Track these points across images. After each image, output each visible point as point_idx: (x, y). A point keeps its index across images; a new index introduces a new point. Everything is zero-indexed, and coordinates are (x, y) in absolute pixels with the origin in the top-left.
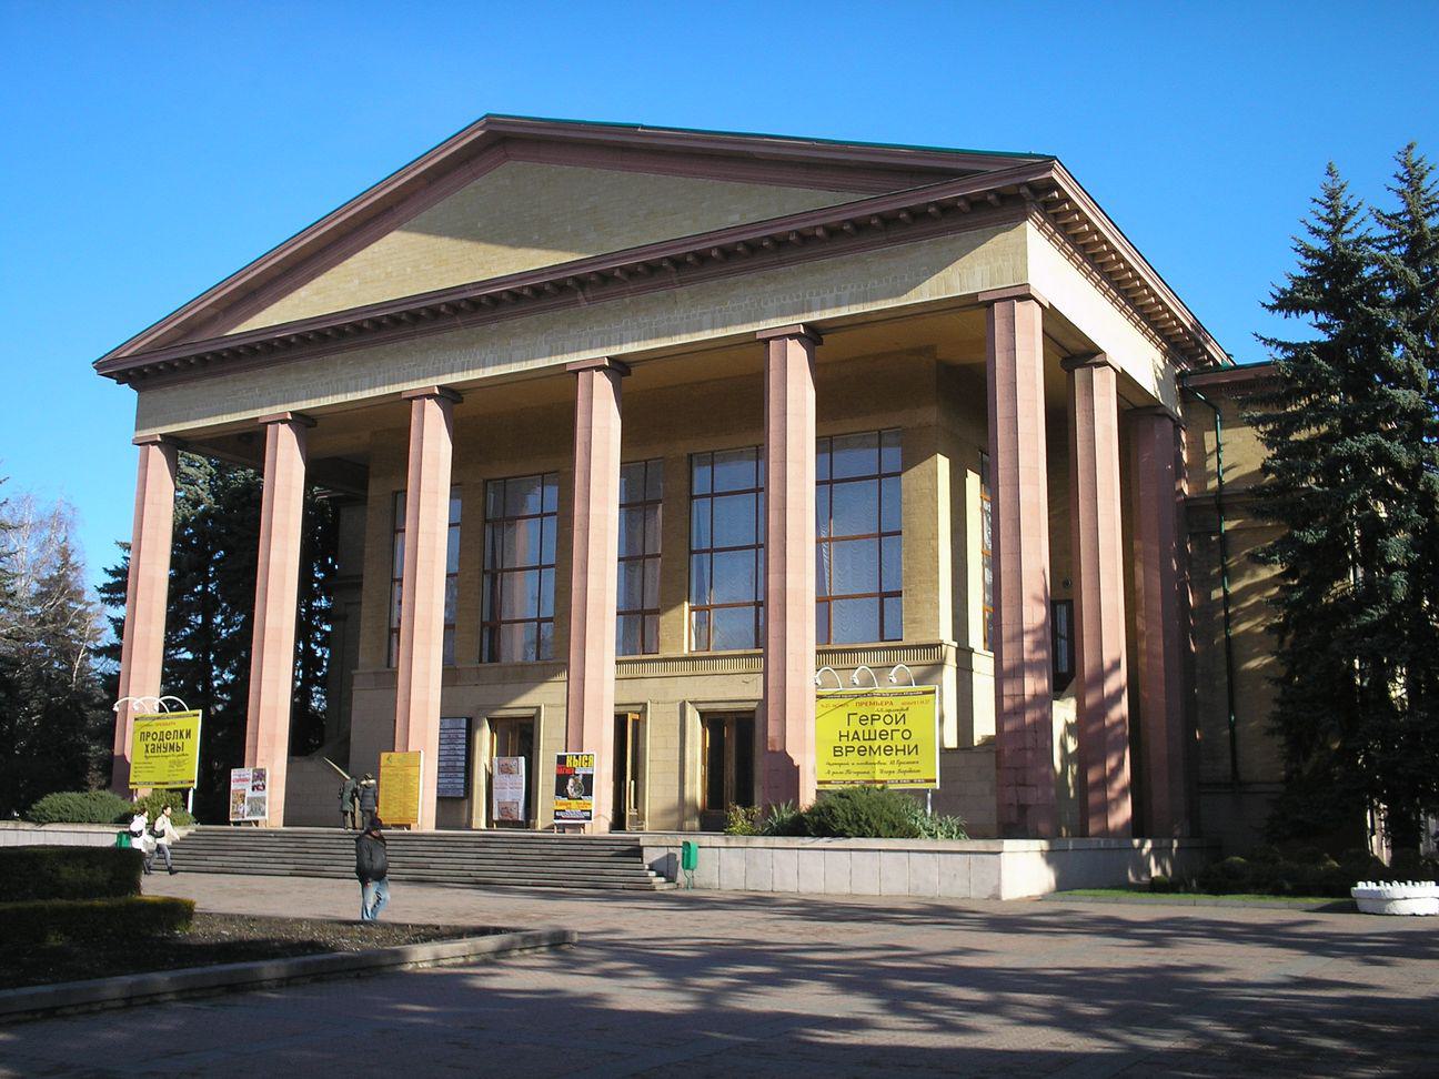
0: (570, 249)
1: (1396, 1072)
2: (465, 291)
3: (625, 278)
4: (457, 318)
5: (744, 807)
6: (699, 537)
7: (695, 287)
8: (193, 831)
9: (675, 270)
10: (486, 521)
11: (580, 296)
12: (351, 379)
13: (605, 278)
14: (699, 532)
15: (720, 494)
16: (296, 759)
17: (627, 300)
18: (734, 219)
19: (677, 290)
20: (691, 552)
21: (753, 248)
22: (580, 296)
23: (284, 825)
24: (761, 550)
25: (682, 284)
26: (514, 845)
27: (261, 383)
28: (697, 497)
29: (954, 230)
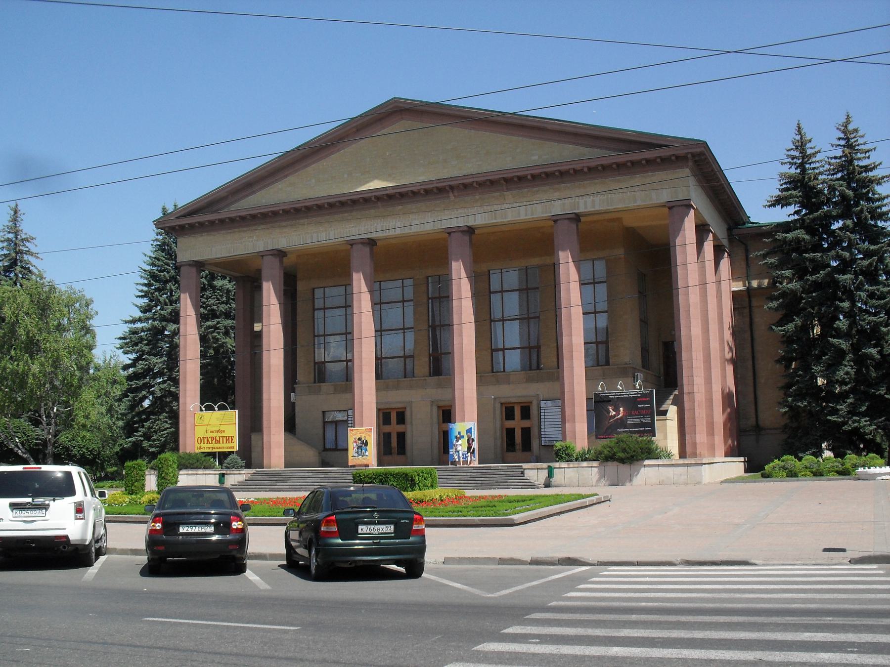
0: (391, 181)
1: (526, 617)
2: (387, 190)
3: (477, 186)
4: (379, 202)
5: (847, 455)
6: (318, 328)
7: (515, 192)
8: (255, 472)
9: (505, 183)
10: (429, 298)
11: (451, 195)
12: (314, 233)
13: (402, 195)
14: (318, 325)
15: (400, 302)
16: (452, 420)
17: (477, 197)
18: (422, 179)
19: (505, 193)
20: (315, 336)
21: (548, 175)
22: (451, 195)
23: (479, 464)
24: (349, 336)
25: (508, 190)
26: (243, 487)
27: (257, 234)
28: (317, 309)
29: (654, 171)
